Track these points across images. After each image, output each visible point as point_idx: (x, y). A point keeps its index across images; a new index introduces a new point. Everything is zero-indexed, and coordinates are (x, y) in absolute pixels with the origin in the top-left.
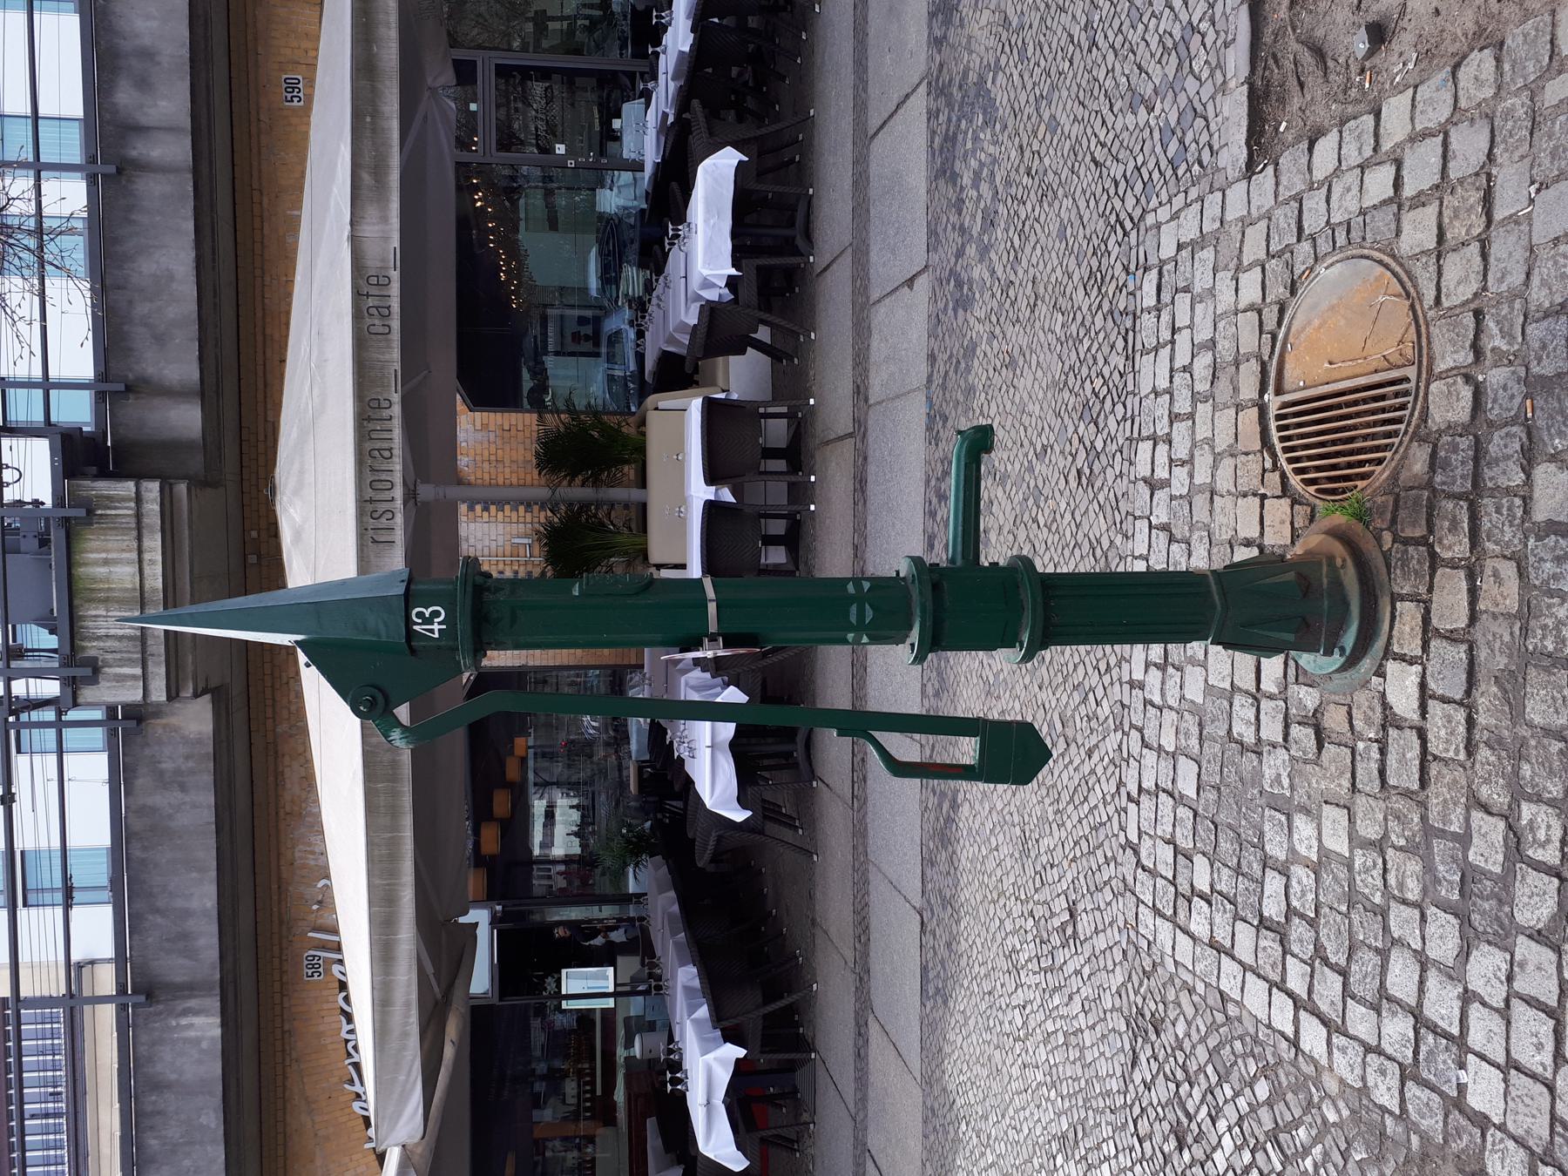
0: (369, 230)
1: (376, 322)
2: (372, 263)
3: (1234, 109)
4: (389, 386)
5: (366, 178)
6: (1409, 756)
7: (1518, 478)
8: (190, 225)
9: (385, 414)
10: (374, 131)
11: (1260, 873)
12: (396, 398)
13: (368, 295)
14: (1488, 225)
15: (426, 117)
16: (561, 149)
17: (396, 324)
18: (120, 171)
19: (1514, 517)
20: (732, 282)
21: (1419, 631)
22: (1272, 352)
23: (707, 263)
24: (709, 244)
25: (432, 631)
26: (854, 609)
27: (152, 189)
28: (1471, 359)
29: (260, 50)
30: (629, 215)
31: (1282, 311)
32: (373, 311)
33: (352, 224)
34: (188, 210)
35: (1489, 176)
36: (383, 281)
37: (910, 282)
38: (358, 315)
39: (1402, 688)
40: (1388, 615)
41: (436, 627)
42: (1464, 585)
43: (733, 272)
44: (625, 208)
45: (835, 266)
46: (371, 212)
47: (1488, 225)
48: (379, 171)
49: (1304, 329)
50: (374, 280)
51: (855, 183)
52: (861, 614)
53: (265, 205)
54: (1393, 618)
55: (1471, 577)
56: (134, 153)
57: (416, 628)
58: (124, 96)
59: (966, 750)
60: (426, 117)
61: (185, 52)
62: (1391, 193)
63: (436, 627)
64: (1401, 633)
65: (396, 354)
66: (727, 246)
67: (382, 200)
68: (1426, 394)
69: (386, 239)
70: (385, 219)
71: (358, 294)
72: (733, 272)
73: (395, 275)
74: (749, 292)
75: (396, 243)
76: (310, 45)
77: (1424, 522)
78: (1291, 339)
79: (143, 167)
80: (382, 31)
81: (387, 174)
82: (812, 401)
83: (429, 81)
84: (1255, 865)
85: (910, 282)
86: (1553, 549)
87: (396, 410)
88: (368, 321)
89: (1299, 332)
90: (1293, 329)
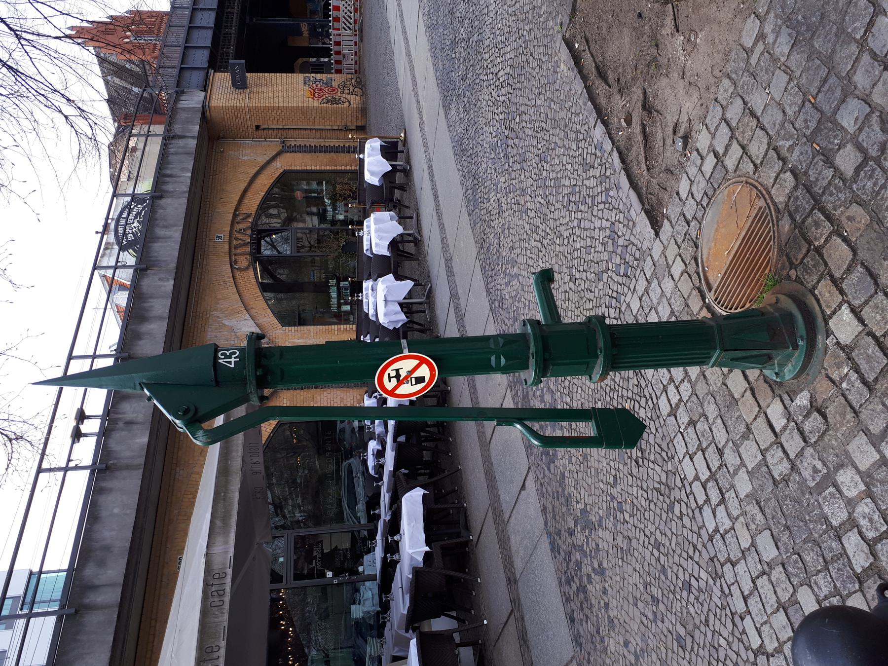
0: (217, 549)
1: (216, 599)
2: (217, 566)
3: (643, 222)
4: (219, 637)
5: (218, 523)
6: (870, 352)
7: (830, 173)
8: (111, 638)
9: (215, 655)
10: (225, 500)
11: (839, 546)
12: (223, 644)
13: (212, 585)
14: (758, 119)
15: (254, 558)
16: (329, 574)
17: (227, 599)
18: (76, 612)
19: (840, 188)
20: (427, 555)
21: (834, 289)
22: (700, 279)
23: (411, 547)
24: (411, 537)
25: (230, 363)
26: (493, 358)
27: (93, 619)
28: (781, 163)
29: (168, 545)
30: (370, 618)
31: (696, 260)
32: (215, 593)
33: (207, 547)
34: (112, 630)
35: (749, 109)
36: (222, 575)
37: (523, 487)
38: (205, 597)
39: (844, 326)
40: (814, 302)
41: (233, 360)
42: (839, 240)
43: (427, 549)
44: (368, 612)
45: (482, 536)
46: (219, 540)
47: (758, 119)
48: (226, 519)
49: (709, 255)
50: (217, 576)
51: (486, 474)
52: (498, 361)
53: (157, 628)
54: (818, 301)
55: (840, 235)
56: (87, 601)
57: (220, 361)
58: (90, 571)
59: (587, 429)
60: (254, 558)
61: (128, 545)
62: (716, 160)
63: (233, 360)
64: (825, 301)
65: (226, 616)
66: (422, 536)
67: (226, 533)
68: (771, 198)
69: (226, 552)
70: (226, 542)
71: (207, 585)
72: (427, 549)
73: (229, 572)
74: (438, 559)
75: (232, 554)
76: (193, 490)
77: (804, 242)
78: (705, 265)
79: (90, 608)
80: (234, 454)
81: (230, 519)
82: (485, 622)
83: (258, 539)
84: (834, 544)
85: (523, 487)
86: (865, 176)
87: (223, 652)
88: (211, 600)
89: (708, 258)
90: (705, 260)
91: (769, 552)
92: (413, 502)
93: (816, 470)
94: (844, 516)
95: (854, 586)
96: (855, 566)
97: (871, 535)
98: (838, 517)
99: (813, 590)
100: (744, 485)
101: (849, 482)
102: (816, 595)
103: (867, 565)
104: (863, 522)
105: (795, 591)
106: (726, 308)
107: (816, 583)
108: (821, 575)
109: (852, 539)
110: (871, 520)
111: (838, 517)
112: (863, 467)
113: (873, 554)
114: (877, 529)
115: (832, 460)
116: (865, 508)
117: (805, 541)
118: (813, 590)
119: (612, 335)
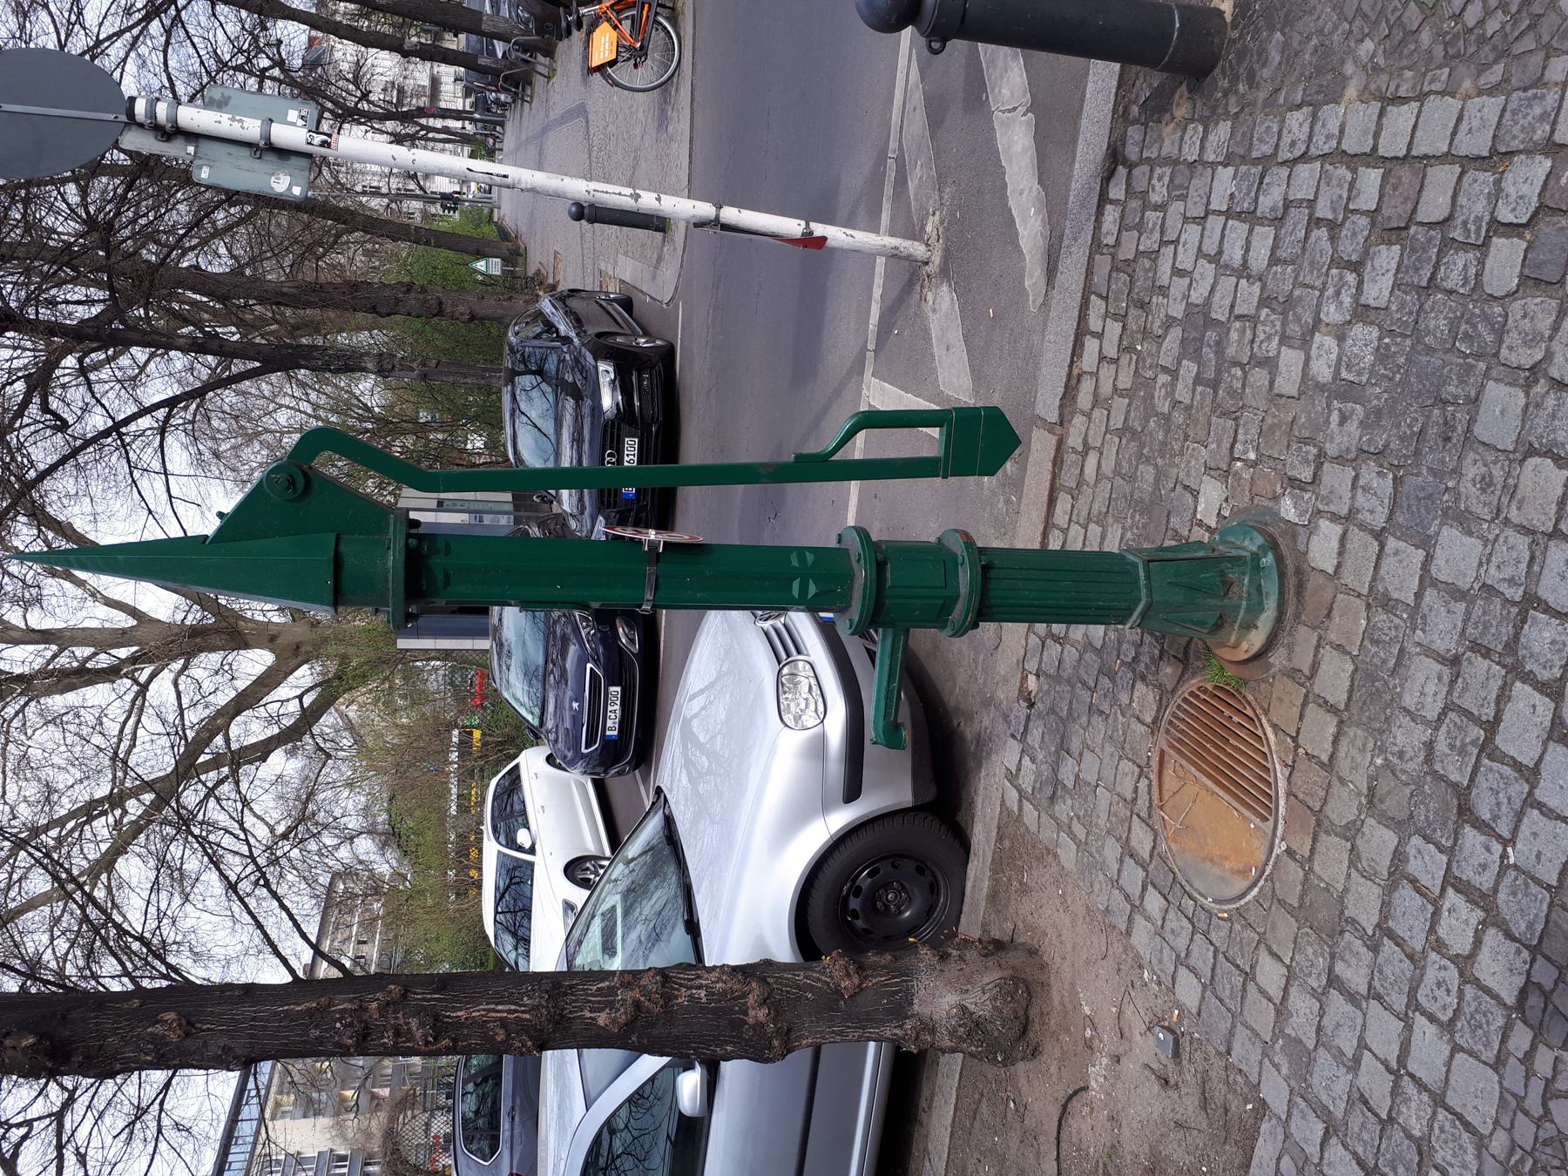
52: (804, 589)
91: (1378, 290)
92: (616, 690)
93: (1344, 419)
94: (1358, 330)
95: (1417, 233)
96: (1397, 259)
97: (1351, 278)
98: (1364, 336)
99: (1478, 275)
100: (1458, 554)
101: (1324, 357)
102: (1481, 263)
103: (1383, 247)
104: (1347, 300)
105: (1511, 295)
106: (1171, 722)
107: (1466, 281)
108: (1449, 285)
109: (1374, 293)
110: (1338, 293)
111: (1364, 336)
112: (1299, 356)
113: (1366, 254)
114: (1341, 278)
115: (1320, 403)
116: (1332, 314)
117: (1430, 350)
118: (1478, 275)
119: (986, 569)
